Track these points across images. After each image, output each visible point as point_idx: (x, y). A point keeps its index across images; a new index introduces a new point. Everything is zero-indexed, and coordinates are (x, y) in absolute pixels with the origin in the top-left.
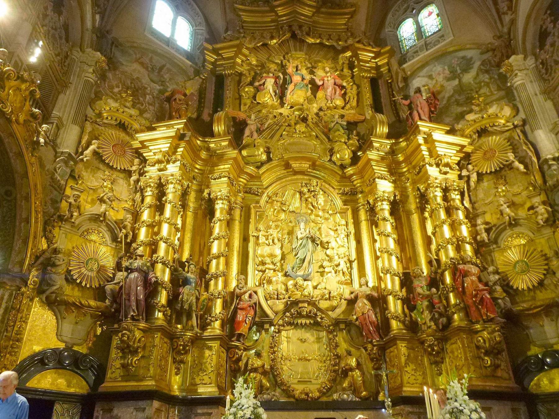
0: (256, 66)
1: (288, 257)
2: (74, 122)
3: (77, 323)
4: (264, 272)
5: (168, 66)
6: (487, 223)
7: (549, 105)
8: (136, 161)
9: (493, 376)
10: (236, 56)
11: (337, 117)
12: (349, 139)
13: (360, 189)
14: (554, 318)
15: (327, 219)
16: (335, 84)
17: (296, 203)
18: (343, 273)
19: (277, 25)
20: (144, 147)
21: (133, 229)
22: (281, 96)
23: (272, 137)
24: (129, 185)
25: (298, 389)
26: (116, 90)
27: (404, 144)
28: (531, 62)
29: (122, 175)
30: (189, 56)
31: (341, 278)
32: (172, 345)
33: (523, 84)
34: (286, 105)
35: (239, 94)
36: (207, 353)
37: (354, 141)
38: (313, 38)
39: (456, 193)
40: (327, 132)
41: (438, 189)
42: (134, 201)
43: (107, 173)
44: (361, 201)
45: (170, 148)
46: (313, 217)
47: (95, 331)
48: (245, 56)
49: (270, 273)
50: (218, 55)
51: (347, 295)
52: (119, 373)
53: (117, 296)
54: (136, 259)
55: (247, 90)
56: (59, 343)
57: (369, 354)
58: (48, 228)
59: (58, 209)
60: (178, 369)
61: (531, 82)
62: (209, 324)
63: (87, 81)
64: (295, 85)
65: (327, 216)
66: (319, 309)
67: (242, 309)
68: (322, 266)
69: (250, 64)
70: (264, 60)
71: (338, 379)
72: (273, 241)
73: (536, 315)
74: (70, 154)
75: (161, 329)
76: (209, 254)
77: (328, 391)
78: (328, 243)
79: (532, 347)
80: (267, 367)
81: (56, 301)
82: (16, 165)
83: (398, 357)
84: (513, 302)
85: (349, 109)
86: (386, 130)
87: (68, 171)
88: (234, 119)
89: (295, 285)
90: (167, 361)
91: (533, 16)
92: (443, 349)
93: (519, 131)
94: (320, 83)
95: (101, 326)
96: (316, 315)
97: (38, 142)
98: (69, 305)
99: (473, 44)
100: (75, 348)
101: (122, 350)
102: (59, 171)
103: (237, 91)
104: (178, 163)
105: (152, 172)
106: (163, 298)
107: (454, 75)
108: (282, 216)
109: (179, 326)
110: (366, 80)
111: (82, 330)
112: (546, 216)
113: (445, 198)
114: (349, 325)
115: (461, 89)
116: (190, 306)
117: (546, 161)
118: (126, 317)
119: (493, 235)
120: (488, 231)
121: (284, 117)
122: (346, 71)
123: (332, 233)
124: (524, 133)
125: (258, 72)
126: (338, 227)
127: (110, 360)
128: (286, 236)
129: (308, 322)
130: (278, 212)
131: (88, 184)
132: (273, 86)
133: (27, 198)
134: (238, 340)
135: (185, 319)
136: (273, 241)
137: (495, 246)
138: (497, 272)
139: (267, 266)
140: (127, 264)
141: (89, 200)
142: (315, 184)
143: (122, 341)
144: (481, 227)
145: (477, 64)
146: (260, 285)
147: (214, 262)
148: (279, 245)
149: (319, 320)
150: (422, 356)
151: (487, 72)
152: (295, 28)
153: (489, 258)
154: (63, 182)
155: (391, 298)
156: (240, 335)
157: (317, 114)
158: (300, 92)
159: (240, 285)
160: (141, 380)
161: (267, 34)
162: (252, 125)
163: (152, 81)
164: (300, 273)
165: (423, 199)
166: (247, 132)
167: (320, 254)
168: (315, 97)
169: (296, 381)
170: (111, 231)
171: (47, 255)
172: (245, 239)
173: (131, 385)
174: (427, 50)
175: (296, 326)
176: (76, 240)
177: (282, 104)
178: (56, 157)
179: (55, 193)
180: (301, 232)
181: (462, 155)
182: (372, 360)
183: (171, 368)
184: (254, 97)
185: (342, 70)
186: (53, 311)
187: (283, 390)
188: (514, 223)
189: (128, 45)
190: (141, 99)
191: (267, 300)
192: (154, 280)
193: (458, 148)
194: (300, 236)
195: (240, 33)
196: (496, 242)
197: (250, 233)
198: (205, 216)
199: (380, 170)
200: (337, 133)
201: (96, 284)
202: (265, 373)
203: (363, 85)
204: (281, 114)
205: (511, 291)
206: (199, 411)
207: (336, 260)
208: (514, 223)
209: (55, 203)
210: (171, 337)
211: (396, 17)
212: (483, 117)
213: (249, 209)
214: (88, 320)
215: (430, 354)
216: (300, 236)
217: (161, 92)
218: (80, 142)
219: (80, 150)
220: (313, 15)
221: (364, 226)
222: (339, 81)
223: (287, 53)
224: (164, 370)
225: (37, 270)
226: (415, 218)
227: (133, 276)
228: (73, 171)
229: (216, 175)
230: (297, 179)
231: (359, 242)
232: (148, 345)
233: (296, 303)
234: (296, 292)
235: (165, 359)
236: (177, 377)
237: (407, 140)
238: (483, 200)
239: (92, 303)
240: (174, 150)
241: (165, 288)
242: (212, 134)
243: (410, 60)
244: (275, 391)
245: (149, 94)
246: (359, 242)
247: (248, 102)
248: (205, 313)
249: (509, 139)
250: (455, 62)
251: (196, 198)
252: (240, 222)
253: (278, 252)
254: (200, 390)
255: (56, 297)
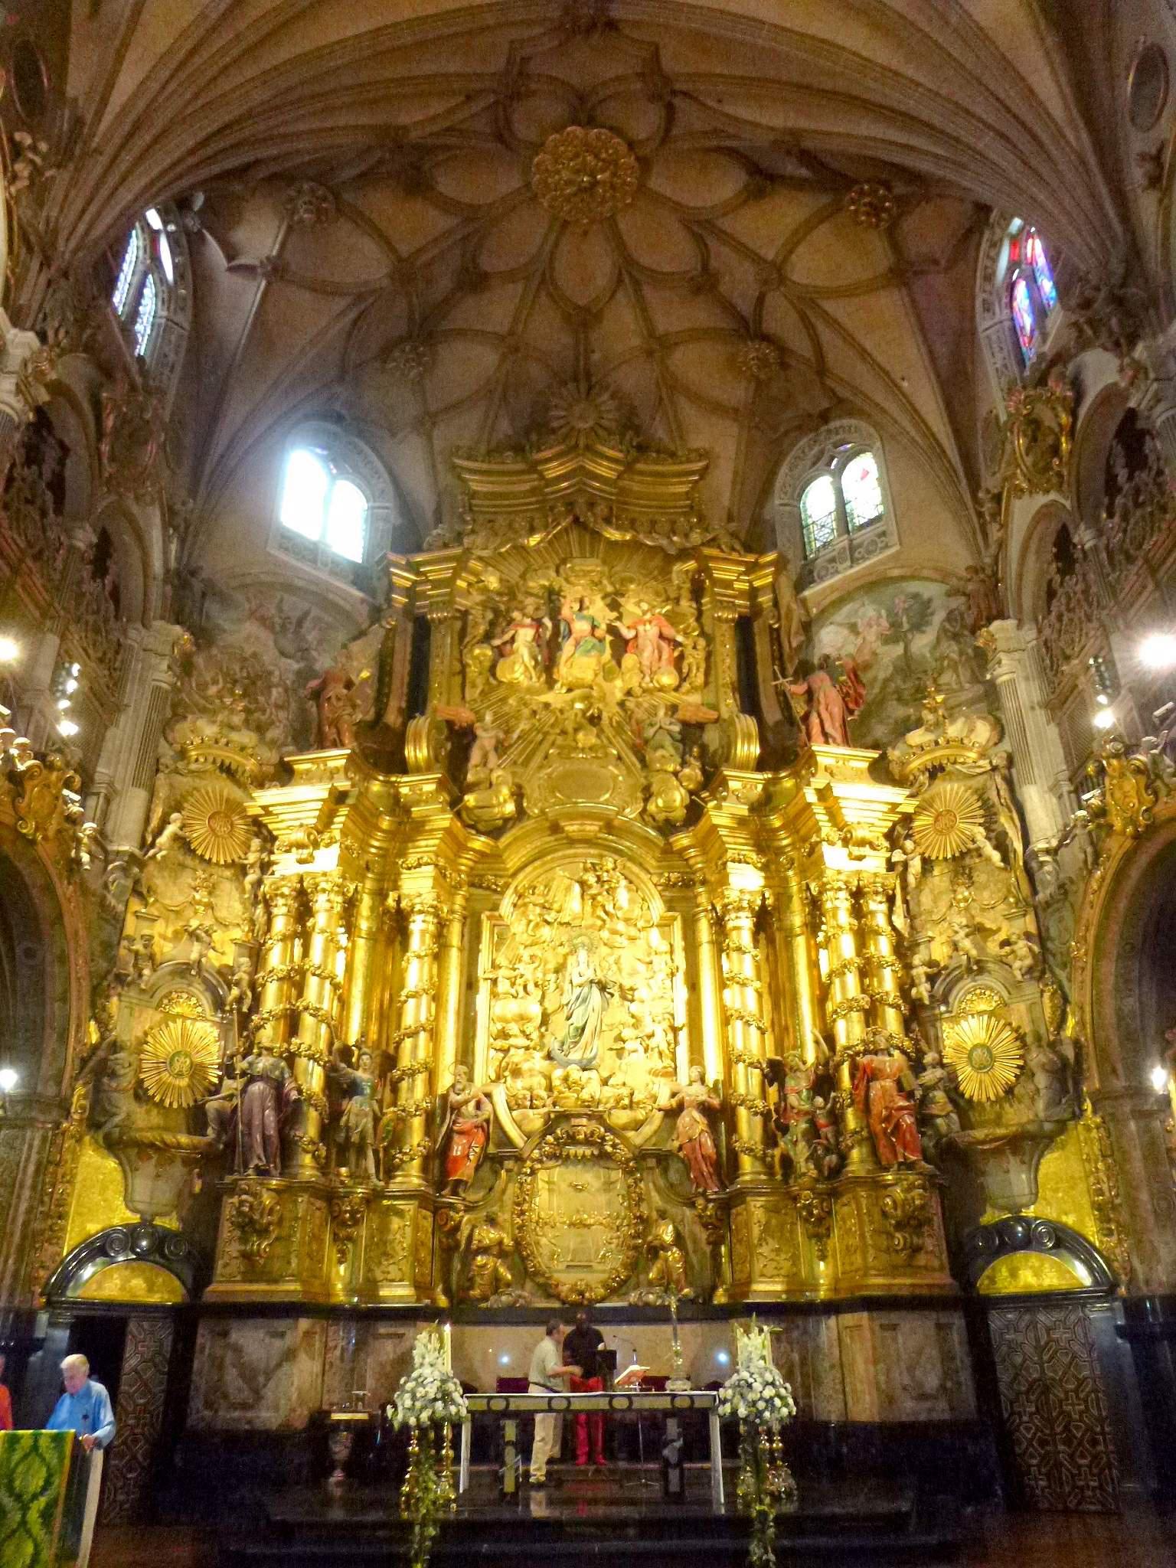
0: (500, 594)
1: (553, 1019)
2: (136, 782)
3: (158, 1176)
4: (506, 1051)
5: (315, 612)
6: (931, 964)
7: (1052, 732)
8: (256, 843)
9: (910, 1267)
10: (456, 575)
11: (661, 713)
12: (684, 764)
13: (699, 876)
14: (1026, 1159)
15: (632, 939)
16: (661, 636)
17: (573, 904)
18: (660, 1054)
19: (544, 501)
20: (268, 813)
21: (253, 986)
22: (548, 665)
23: (526, 763)
24: (243, 891)
25: (567, 1281)
26: (213, 690)
27: (788, 783)
28: (1029, 634)
29: (228, 873)
30: (359, 576)
31: (658, 1064)
32: (331, 1212)
33: (1012, 681)
34: (558, 686)
35: (461, 661)
36: (396, 1223)
37: (693, 772)
38: (618, 528)
39: (879, 898)
40: (640, 751)
41: (844, 895)
42: (252, 922)
43: (200, 873)
44: (703, 899)
45: (319, 818)
46: (605, 934)
47: (191, 1185)
48: (476, 574)
49: (516, 1056)
50: (418, 573)
51: (664, 1101)
52: (237, 1266)
53: (226, 1121)
54: (259, 1055)
55: (477, 651)
56: (129, 1214)
57: (700, 1217)
58: (99, 1002)
59: (113, 960)
60: (343, 1252)
61: (1027, 679)
62: (398, 1168)
63: (159, 688)
64: (577, 644)
65: (633, 932)
66: (609, 1129)
67: (461, 1133)
68: (619, 1038)
69: (485, 590)
70: (514, 578)
71: (642, 1263)
72: (525, 987)
73: (997, 1152)
74: (132, 855)
75: (308, 1188)
76: (399, 1027)
77: (616, 1289)
78: (632, 989)
79: (989, 1210)
80: (508, 1241)
81: (120, 1141)
82: (45, 909)
83: (747, 1225)
84: (966, 1124)
85: (688, 692)
86: (755, 750)
87: (129, 883)
88: (450, 724)
89: (566, 1079)
90: (321, 1242)
91: (1033, 546)
92: (829, 1213)
93: (999, 779)
94: (628, 634)
95: (200, 1176)
96: (603, 1138)
97: (78, 861)
98: (145, 1148)
99: (936, 569)
100: (158, 1222)
101: (241, 1227)
102: (112, 888)
103: (456, 653)
104: (335, 849)
105: (286, 865)
106: (310, 1128)
107: (895, 634)
108: (546, 932)
109: (344, 1170)
110: (725, 626)
111: (165, 1192)
112: (1029, 961)
113: (858, 912)
114: (663, 1159)
115: (907, 667)
116: (363, 1136)
117: (1035, 854)
118: (246, 1167)
119: (940, 987)
120: (931, 979)
121: (553, 712)
122: (686, 605)
123: (642, 967)
124: (1009, 782)
125: (503, 607)
126: (654, 958)
127: (220, 1243)
128: (552, 977)
129: (588, 1152)
130: (537, 925)
131: (167, 902)
132: (530, 649)
133: (63, 959)
134: (455, 1193)
135: (353, 1158)
136: (525, 987)
137: (943, 1008)
138: (941, 1064)
139: (512, 1041)
140: (244, 1065)
141: (169, 934)
142: (610, 865)
143: (240, 1213)
144: (920, 972)
145: (939, 617)
146: (499, 1077)
147: (408, 1043)
148: (536, 994)
149: (609, 1149)
150: (793, 1224)
151: (956, 637)
152: (580, 508)
153: (932, 1032)
154: (120, 908)
155: (743, 1112)
156: (458, 1182)
157: (622, 704)
158: (585, 660)
159: (459, 1086)
160: (276, 1281)
161: (521, 523)
162: (486, 738)
163: (283, 654)
164: (576, 1055)
165: (815, 905)
166: (475, 756)
167: (618, 1012)
168: (619, 664)
169: (562, 1266)
170: (211, 989)
171: (101, 1054)
172: (470, 985)
173: (258, 1290)
174: (854, 561)
175: (566, 1160)
176: (149, 1017)
177: (550, 683)
178: (107, 862)
179: (109, 928)
180: (581, 968)
181: (896, 818)
182: (705, 1226)
183: (330, 1252)
184: (492, 670)
185: (677, 600)
186: (117, 1157)
187: (539, 1285)
188: (977, 967)
189: (234, 583)
190: (261, 699)
191: (511, 1109)
192: (294, 1095)
193: (886, 808)
194: (577, 981)
195: (466, 522)
196: (945, 1000)
197: (480, 974)
198: (390, 942)
199: (737, 845)
200: (660, 753)
201: (187, 1101)
202: (502, 1254)
203: (718, 639)
204: (547, 706)
205: (962, 1103)
206: (382, 1331)
207: (648, 1027)
208: (977, 967)
209: (109, 948)
210: (330, 1197)
211: (796, 472)
212: (937, 743)
213: (478, 924)
214: (178, 1170)
215: (806, 1220)
216: (577, 981)
217: (304, 676)
218: (147, 820)
219: (149, 839)
220: (619, 477)
221: (706, 953)
222: (669, 631)
223: (564, 561)
224: (316, 1258)
225: (85, 1084)
226: (800, 943)
227: (257, 1087)
228: (137, 882)
229: (412, 859)
230: (575, 856)
231: (693, 986)
232: (287, 1215)
233: (564, 1117)
234: (567, 1094)
235: (317, 1238)
236: (342, 1269)
237: (796, 775)
238: (931, 912)
239: (184, 1139)
240: (327, 819)
241: (316, 1106)
242: (402, 767)
243: (822, 579)
244: (523, 1287)
245: (277, 686)
246: (693, 986)
247: (480, 682)
248: (391, 1145)
249: (981, 795)
250: (900, 603)
251: (372, 909)
252: (461, 950)
253: (536, 1012)
254: (384, 1292)
255: (121, 1134)
